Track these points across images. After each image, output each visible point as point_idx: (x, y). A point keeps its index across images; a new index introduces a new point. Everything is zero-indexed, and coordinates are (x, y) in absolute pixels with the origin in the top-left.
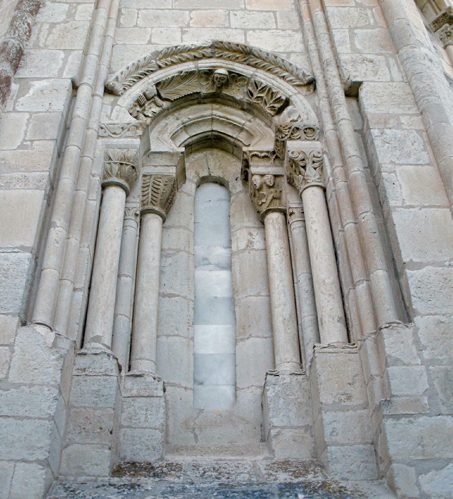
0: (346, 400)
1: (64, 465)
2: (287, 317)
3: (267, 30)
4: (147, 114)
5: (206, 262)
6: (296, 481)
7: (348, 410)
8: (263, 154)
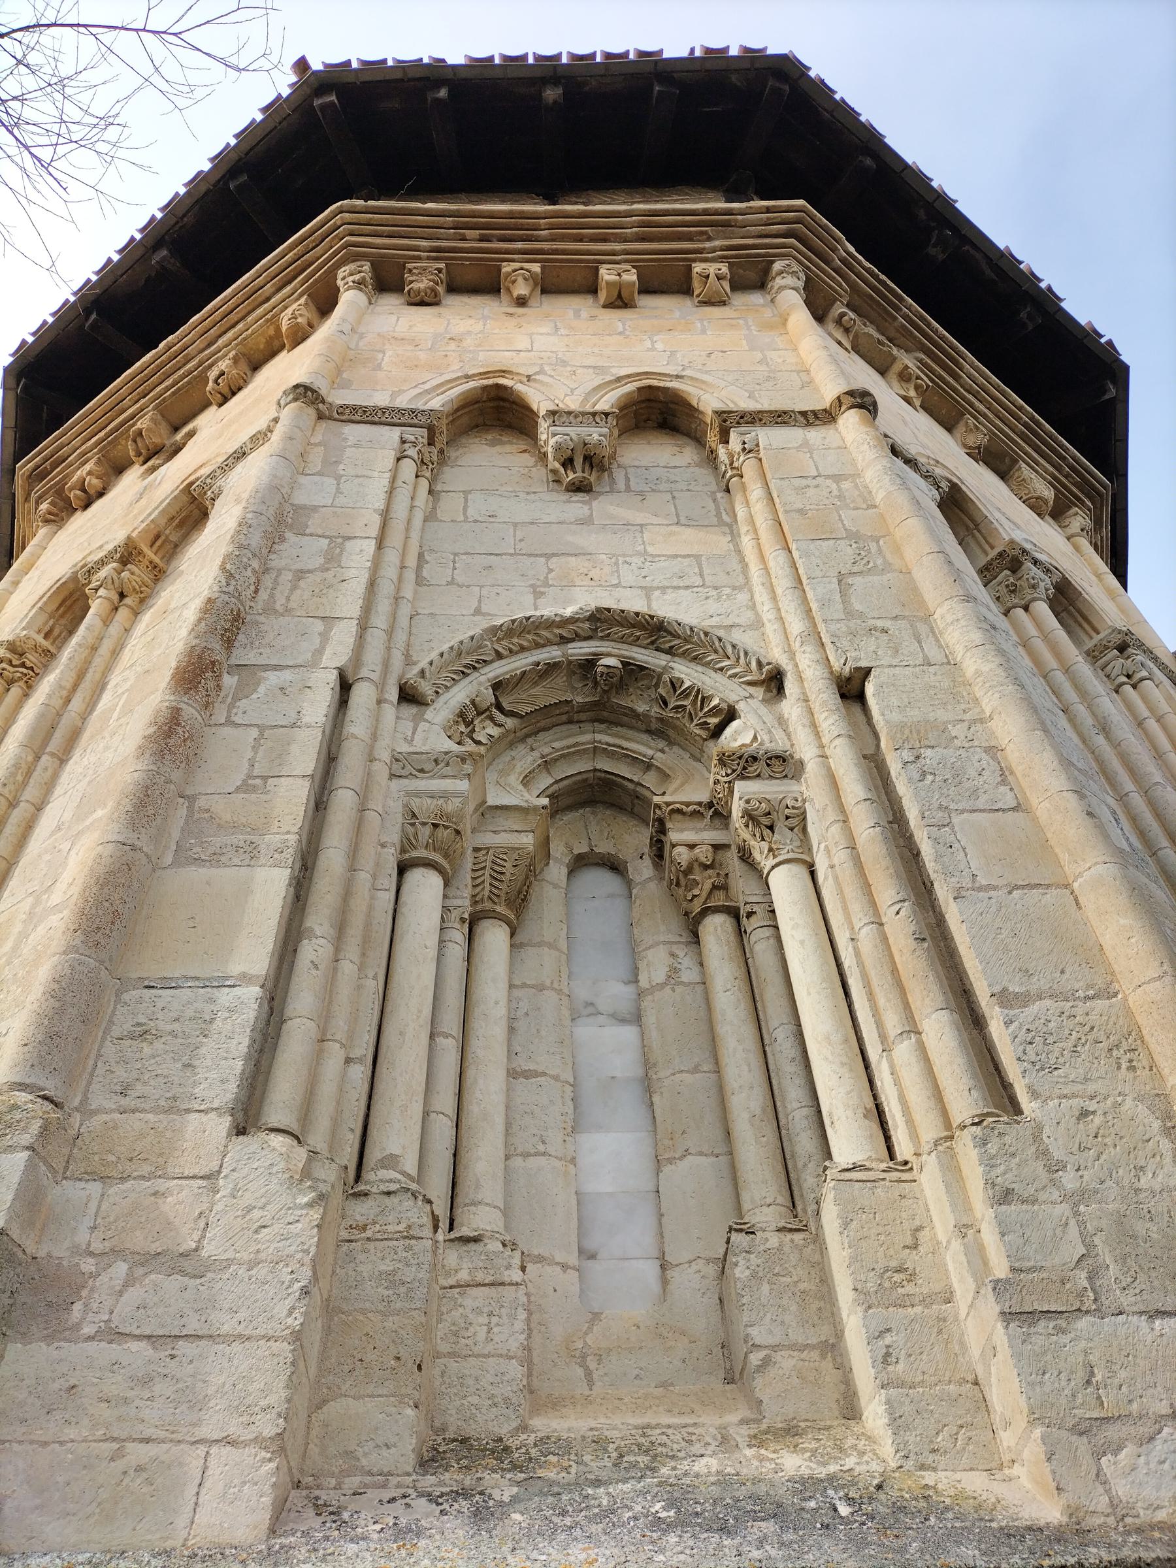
0: (905, 1283)
1: (313, 1449)
2: (758, 1112)
3: (688, 587)
4: (478, 739)
5: (590, 1010)
6: (822, 1472)
7: (913, 1306)
8: (691, 808)
